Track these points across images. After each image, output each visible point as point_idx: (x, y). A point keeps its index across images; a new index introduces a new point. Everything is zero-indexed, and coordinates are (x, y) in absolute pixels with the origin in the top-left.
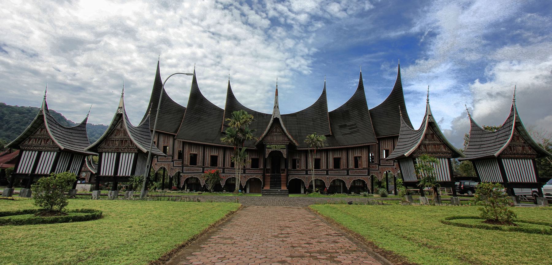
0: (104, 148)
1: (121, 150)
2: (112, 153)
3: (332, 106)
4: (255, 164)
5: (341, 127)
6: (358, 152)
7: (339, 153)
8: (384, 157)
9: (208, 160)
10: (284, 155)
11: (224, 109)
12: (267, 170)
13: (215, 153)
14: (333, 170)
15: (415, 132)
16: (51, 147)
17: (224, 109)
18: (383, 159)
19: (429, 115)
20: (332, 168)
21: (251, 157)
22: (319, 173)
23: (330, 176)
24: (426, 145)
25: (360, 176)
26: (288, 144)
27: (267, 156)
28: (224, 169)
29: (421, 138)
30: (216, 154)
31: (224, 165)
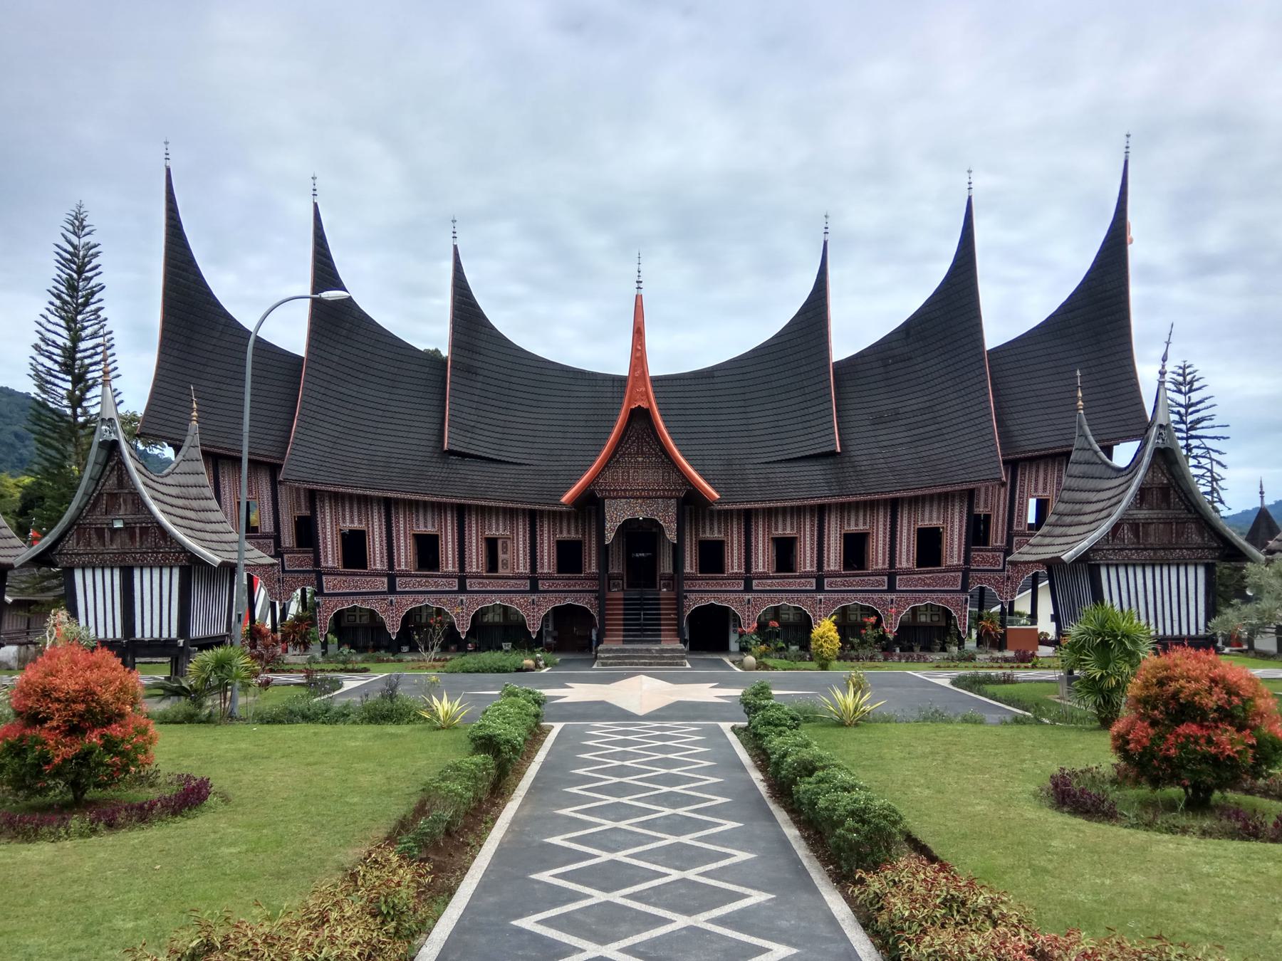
0: (77, 554)
1: (134, 558)
2: (103, 569)
3: (842, 347)
4: (569, 557)
5: (878, 420)
7: (865, 516)
9: (405, 555)
10: (667, 532)
12: (611, 578)
13: (427, 526)
14: (840, 576)
15: (1109, 473)
19: (1161, 426)
20: (837, 568)
21: (555, 535)
22: (789, 584)
23: (756, 595)
24: (1137, 525)
27: (610, 536)
28: (466, 577)
29: (1124, 503)
30: (430, 530)
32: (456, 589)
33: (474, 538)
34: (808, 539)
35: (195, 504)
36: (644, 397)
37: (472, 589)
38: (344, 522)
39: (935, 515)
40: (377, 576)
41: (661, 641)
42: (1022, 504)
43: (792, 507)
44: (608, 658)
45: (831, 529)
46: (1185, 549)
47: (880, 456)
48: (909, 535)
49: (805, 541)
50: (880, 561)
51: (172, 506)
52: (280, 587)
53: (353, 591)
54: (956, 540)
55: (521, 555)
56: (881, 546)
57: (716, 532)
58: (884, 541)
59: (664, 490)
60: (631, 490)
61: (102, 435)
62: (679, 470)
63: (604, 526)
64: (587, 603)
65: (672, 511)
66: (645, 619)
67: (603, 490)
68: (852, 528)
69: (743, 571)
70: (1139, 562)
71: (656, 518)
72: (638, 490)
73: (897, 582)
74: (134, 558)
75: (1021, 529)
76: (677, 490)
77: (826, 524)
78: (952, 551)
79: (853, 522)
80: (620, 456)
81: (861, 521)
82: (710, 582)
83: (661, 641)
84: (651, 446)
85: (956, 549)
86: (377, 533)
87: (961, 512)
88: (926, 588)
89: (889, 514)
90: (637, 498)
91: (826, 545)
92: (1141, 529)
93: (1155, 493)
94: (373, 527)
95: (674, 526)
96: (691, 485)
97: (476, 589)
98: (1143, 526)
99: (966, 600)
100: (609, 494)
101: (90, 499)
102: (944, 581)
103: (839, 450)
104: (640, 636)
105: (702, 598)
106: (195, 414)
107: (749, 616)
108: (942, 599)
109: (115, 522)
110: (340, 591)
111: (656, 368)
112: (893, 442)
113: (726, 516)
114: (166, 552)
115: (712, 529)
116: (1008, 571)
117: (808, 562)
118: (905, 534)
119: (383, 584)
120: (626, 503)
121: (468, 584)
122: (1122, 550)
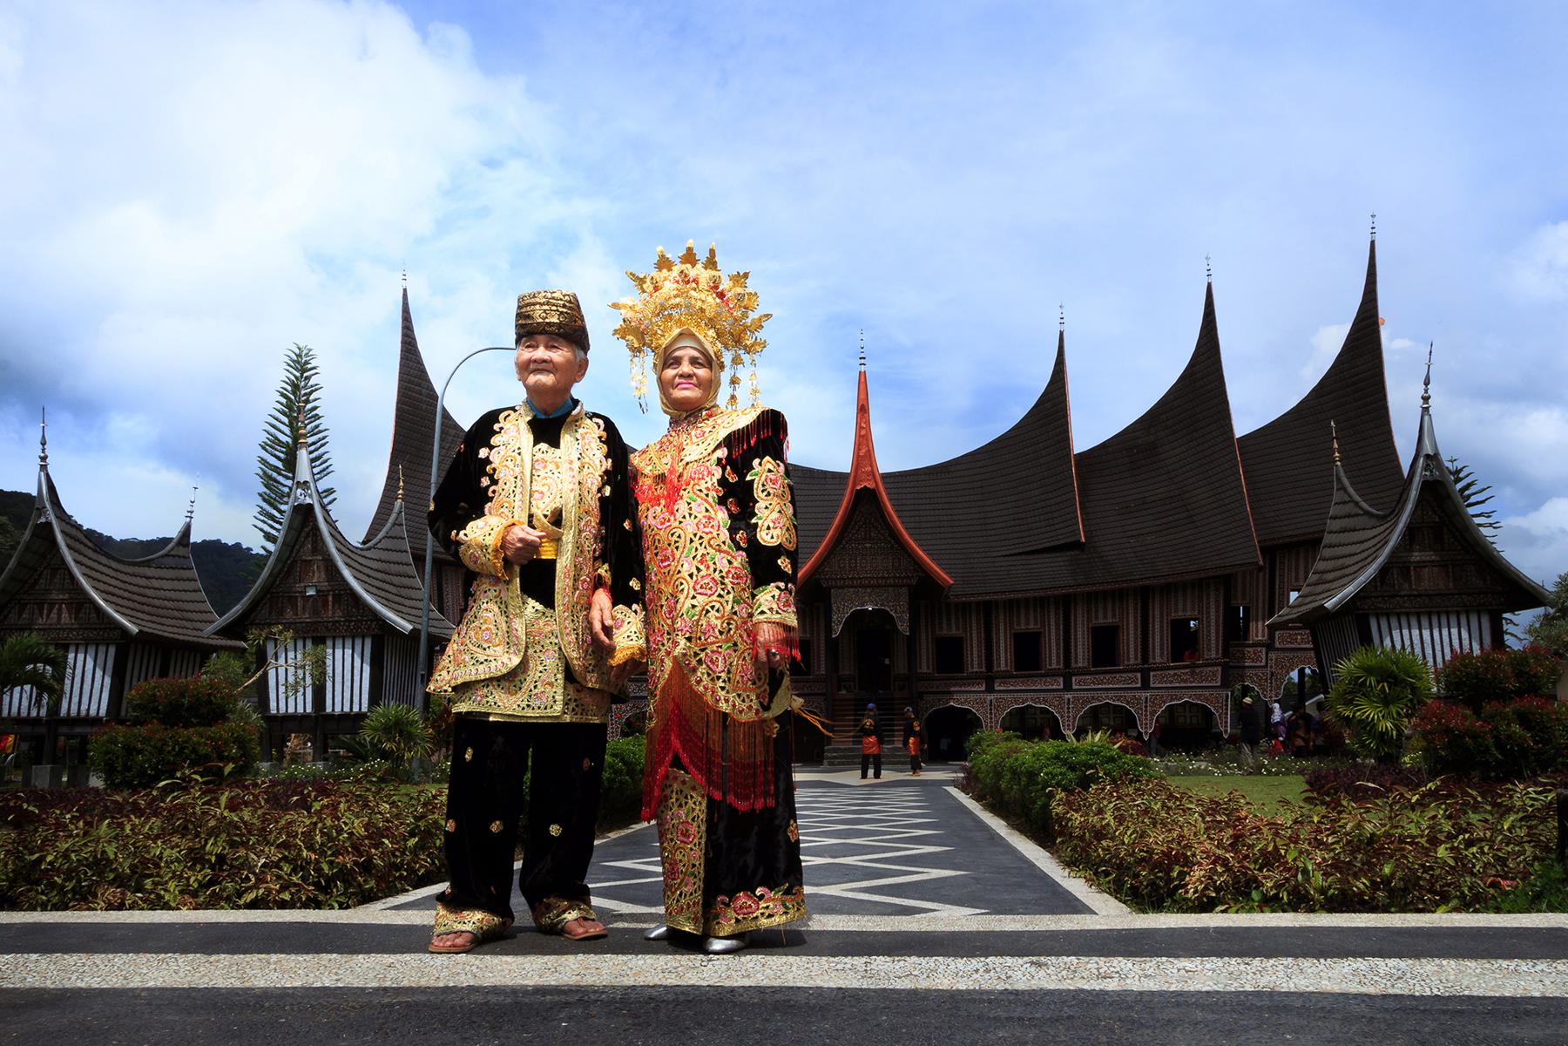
1: (327, 627)
3: (1087, 431)
16: (95, 629)
19: (1428, 456)
20: (1086, 664)
26: (914, 582)
27: (837, 630)
31: (1145, 659)
34: (1053, 634)
35: (396, 580)
36: (870, 478)
42: (1283, 595)
43: (1035, 599)
44: (835, 757)
46: (1465, 594)
47: (1127, 545)
48: (1162, 627)
49: (1050, 635)
50: (1132, 656)
51: (361, 564)
57: (954, 628)
61: (296, 498)
62: (910, 556)
63: (831, 618)
64: (816, 707)
65: (904, 603)
69: (984, 670)
70: (1413, 610)
72: (867, 578)
74: (327, 627)
77: (1073, 618)
78: (1209, 645)
79: (1101, 615)
81: (1110, 614)
87: (1217, 601)
88: (1183, 685)
89: (1139, 605)
90: (865, 587)
92: (1412, 573)
93: (1426, 533)
95: (906, 616)
96: (924, 571)
98: (1415, 569)
99: (1227, 696)
101: (284, 566)
103: (1083, 540)
105: (940, 700)
106: (400, 492)
107: (991, 718)
109: (307, 589)
111: (887, 463)
112: (1143, 531)
113: (964, 609)
114: (358, 621)
115: (949, 625)
117: (1054, 658)
122: (1393, 597)
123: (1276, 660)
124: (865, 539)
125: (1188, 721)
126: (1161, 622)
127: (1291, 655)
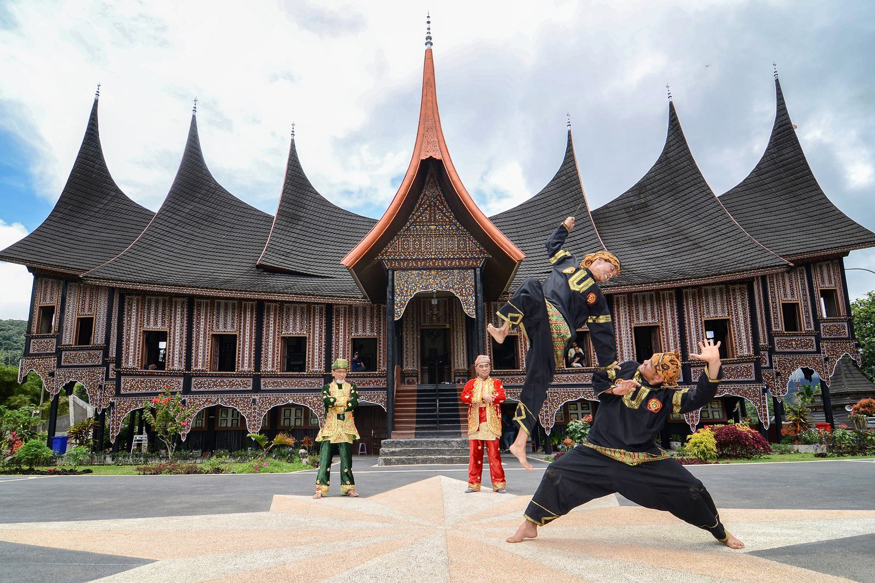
6: (715, 305)
8: (825, 316)
10: (464, 307)
11: (273, 213)
13: (294, 329)
17: (273, 213)
18: (825, 321)
25: (732, 387)
28: (260, 377)
30: (229, 330)
31: (188, 365)
32: (250, 388)
33: (271, 337)
37: (267, 388)
38: (148, 324)
39: (719, 308)
40: (174, 376)
41: (460, 433)
44: (393, 453)
45: (622, 323)
48: (697, 327)
52: (101, 393)
53: (150, 391)
54: (743, 331)
55: (316, 354)
56: (671, 338)
58: (674, 333)
59: (460, 259)
60: (424, 260)
64: (381, 401)
66: (440, 411)
67: (392, 259)
68: (642, 322)
71: (451, 290)
73: (692, 375)
75: (778, 330)
76: (474, 258)
80: (411, 225)
82: (505, 377)
83: (460, 433)
84: (444, 214)
85: (744, 340)
86: (178, 335)
90: (430, 269)
91: (618, 339)
94: (175, 328)
97: (270, 388)
100: (399, 264)
102: (737, 372)
104: (435, 428)
108: (739, 390)
110: (137, 392)
116: (776, 368)
117: (246, 362)
118: (693, 326)
119: (178, 384)
120: (418, 275)
121: (262, 384)
123: (779, 361)
124: (430, 221)
125: (292, 424)
126: (696, 323)
127: (790, 357)
